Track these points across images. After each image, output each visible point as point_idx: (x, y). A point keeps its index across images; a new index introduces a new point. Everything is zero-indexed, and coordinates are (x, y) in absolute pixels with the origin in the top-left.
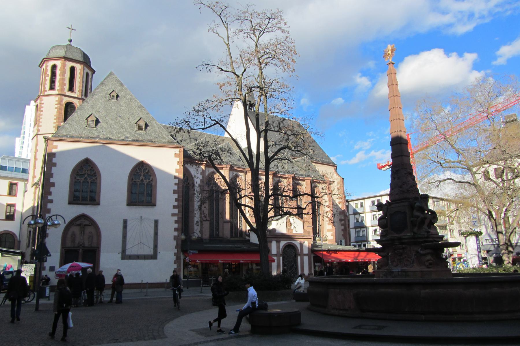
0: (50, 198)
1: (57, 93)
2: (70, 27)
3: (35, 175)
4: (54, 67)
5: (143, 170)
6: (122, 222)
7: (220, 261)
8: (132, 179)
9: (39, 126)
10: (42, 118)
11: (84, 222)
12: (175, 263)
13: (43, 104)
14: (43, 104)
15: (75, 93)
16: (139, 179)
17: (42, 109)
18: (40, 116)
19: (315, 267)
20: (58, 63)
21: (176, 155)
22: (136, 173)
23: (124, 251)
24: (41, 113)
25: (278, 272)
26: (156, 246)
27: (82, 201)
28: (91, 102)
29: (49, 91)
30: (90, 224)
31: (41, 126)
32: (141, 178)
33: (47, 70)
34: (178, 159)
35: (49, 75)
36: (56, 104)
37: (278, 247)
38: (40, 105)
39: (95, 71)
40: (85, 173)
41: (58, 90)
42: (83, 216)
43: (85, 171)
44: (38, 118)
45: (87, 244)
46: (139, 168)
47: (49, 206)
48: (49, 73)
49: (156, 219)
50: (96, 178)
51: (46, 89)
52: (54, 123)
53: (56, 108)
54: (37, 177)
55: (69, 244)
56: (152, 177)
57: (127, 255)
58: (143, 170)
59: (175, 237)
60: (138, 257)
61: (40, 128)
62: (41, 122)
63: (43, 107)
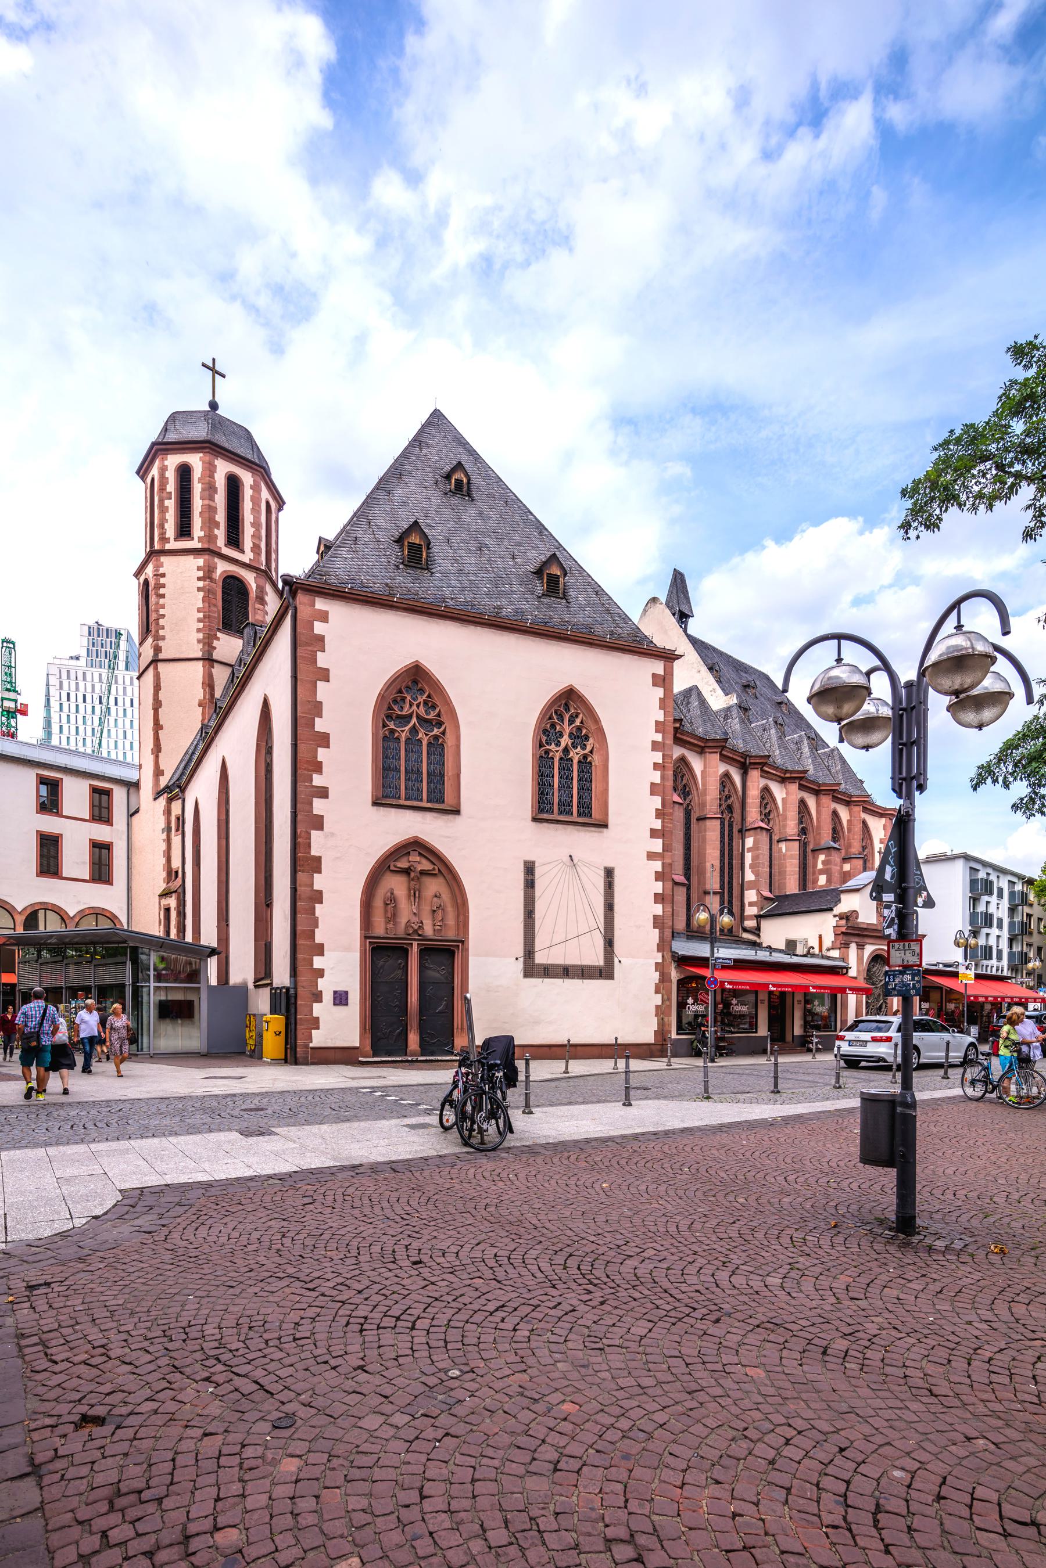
0: (317, 780)
1: (199, 546)
3: (161, 768)
4: (184, 473)
5: (567, 717)
6: (521, 868)
7: (812, 990)
8: (541, 745)
10: (163, 616)
11: (419, 863)
13: (163, 575)
14: (163, 575)
15: (243, 552)
16: (558, 744)
17: (162, 591)
18: (157, 611)
23: (529, 953)
24: (162, 601)
26: (609, 943)
27: (406, 799)
28: (400, 491)
29: (175, 540)
30: (434, 869)
31: (163, 638)
32: (563, 744)
36: (199, 579)
37: (860, 959)
38: (157, 580)
40: (410, 716)
41: (200, 539)
42: (416, 846)
43: (411, 706)
44: (153, 616)
46: (556, 712)
47: (319, 806)
48: (171, 487)
49: (610, 865)
50: (441, 730)
52: (199, 630)
53: (199, 589)
55: (380, 929)
56: (591, 740)
57: (540, 965)
58: (567, 717)
59: (656, 918)
60: (566, 972)
61: (161, 643)
63: (163, 586)
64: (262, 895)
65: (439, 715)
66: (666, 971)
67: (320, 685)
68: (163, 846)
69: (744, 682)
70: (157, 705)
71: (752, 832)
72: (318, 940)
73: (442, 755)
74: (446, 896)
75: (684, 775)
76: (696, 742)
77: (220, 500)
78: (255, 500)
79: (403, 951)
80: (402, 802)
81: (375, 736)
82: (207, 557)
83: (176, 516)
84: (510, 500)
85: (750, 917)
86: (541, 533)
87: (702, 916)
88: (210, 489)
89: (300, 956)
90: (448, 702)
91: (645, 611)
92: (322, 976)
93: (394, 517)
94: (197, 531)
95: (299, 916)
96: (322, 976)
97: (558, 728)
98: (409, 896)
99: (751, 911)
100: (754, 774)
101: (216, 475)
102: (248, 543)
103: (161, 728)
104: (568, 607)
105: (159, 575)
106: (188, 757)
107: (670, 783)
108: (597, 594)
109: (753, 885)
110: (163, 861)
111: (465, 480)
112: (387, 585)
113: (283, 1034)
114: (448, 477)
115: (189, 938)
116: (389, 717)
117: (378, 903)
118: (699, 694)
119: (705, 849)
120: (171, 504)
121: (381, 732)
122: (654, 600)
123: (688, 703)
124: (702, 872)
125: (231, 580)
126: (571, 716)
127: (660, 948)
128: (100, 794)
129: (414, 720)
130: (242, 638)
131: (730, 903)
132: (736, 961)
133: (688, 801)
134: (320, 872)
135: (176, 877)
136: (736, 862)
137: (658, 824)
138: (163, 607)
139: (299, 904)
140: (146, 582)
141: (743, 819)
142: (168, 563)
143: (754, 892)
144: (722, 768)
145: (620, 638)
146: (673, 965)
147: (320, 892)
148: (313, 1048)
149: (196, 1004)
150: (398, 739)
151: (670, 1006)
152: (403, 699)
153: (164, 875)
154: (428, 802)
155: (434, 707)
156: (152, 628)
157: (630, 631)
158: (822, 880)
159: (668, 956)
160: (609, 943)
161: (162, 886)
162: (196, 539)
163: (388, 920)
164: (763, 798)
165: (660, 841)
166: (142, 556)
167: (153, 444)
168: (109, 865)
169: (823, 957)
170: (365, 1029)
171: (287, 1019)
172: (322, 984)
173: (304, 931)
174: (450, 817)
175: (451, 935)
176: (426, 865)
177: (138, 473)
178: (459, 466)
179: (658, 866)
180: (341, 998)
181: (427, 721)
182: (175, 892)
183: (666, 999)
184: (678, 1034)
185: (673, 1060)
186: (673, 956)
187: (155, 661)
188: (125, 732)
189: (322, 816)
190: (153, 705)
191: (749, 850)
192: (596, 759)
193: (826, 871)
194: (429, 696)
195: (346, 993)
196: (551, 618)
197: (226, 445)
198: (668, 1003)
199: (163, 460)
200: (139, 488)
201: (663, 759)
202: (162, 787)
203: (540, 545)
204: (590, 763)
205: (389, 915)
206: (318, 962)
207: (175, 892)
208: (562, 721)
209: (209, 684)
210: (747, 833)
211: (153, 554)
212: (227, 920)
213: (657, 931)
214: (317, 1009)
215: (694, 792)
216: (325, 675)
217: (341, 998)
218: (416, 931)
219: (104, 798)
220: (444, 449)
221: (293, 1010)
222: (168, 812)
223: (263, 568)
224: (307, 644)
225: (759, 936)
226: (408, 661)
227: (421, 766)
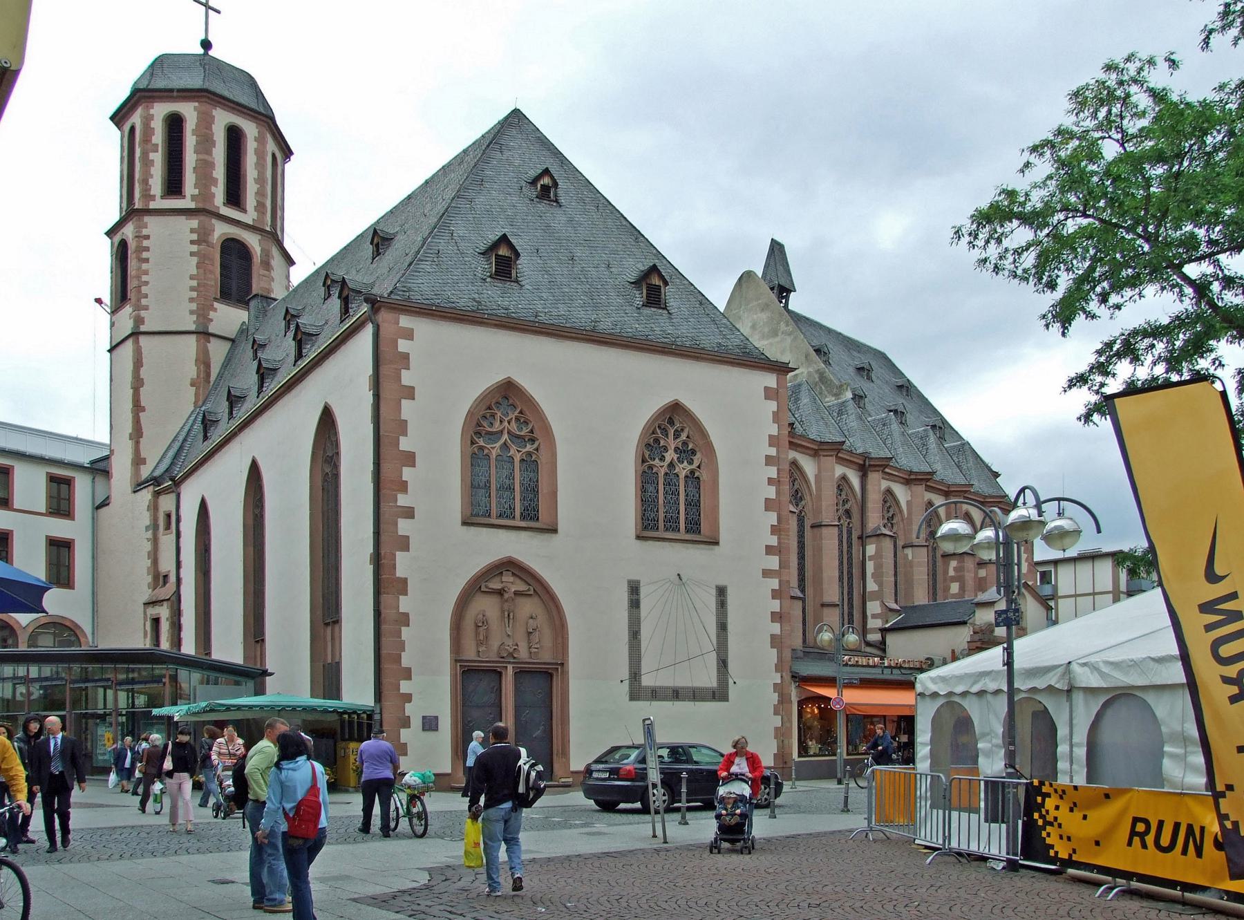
1: (192, 205)
3: (143, 455)
4: (175, 124)
5: (671, 432)
8: (643, 461)
10: (146, 283)
13: (147, 237)
15: (244, 211)
16: (662, 459)
17: (145, 255)
18: (138, 277)
20: (189, 111)
21: (769, 394)
23: (635, 675)
24: (144, 266)
25: (475, 748)
26: (723, 664)
27: (497, 518)
28: (482, 199)
29: (162, 197)
30: (529, 590)
31: (146, 308)
33: (148, 131)
35: (157, 145)
36: (192, 242)
39: (291, 153)
40: (502, 432)
41: (193, 198)
44: (132, 284)
45: (523, 654)
46: (659, 427)
48: (158, 138)
49: (721, 583)
50: (535, 446)
51: (152, 193)
52: (191, 300)
53: (192, 254)
56: (698, 455)
58: (671, 432)
61: (143, 313)
65: (532, 431)
68: (148, 546)
69: (858, 363)
71: (874, 539)
74: (542, 620)
76: (809, 445)
77: (219, 154)
78: (260, 154)
82: (202, 218)
85: (873, 631)
87: (826, 636)
92: (410, 701)
98: (503, 617)
99: (873, 623)
100: (873, 477)
102: (250, 200)
103: (143, 409)
105: (140, 237)
107: (786, 497)
109: (878, 596)
110: (149, 563)
112: (474, 299)
114: (534, 182)
115: (165, 645)
120: (158, 158)
124: (818, 581)
126: (676, 431)
129: (505, 436)
131: (851, 615)
133: (800, 507)
136: (856, 571)
137: (774, 541)
138: (146, 273)
142: (153, 225)
143: (878, 603)
144: (839, 470)
147: (406, 615)
152: (493, 416)
153: (149, 579)
156: (131, 295)
157: (737, 342)
158: (955, 588)
159: (788, 677)
160: (723, 664)
161: (146, 594)
163: (479, 643)
164: (885, 501)
165: (776, 559)
168: (70, 568)
172: (409, 709)
174: (546, 536)
175: (546, 657)
176: (521, 587)
178: (546, 172)
179: (774, 583)
181: (518, 437)
183: (786, 721)
185: (797, 783)
187: (135, 334)
189: (408, 537)
191: (871, 558)
192: (704, 475)
193: (959, 579)
194: (521, 412)
195: (436, 718)
197: (226, 93)
199: (148, 108)
200: (114, 136)
201: (778, 474)
204: (698, 478)
205: (481, 638)
208: (667, 435)
209: (204, 362)
210: (868, 540)
211: (131, 213)
215: (807, 497)
218: (511, 655)
219: (64, 487)
222: (154, 507)
223: (268, 229)
226: (499, 377)
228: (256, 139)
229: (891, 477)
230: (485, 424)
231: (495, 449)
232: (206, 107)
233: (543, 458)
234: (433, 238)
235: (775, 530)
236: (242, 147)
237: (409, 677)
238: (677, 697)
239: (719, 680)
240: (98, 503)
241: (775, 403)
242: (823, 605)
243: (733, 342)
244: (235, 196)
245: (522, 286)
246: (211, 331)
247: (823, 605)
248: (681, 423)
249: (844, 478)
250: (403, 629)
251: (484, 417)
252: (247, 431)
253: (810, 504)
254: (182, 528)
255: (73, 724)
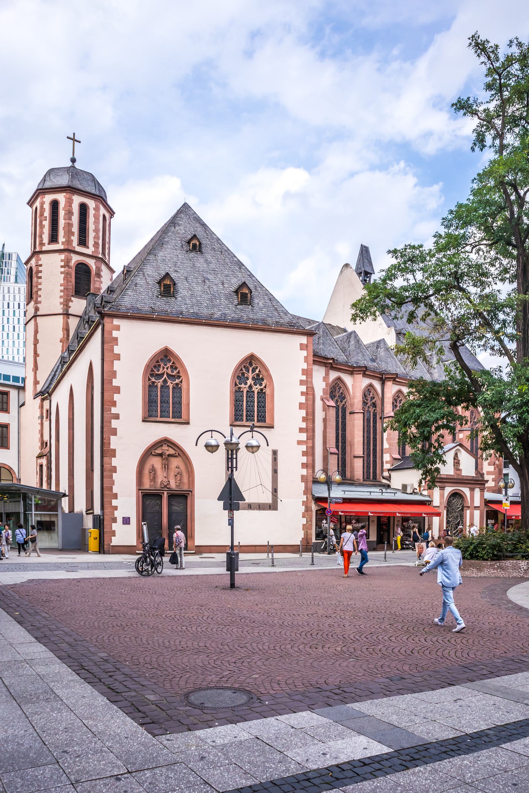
0: (114, 410)
2: (72, 137)
3: (38, 380)
4: (55, 205)
5: (251, 369)
7: (398, 515)
8: (236, 385)
9: (37, 302)
10: (40, 289)
12: (304, 516)
13: (41, 265)
14: (41, 265)
15: (88, 248)
16: (246, 384)
17: (40, 275)
19: (487, 525)
21: (302, 347)
22: (240, 374)
24: (40, 280)
26: (275, 491)
27: (161, 417)
28: (161, 254)
29: (48, 244)
30: (176, 453)
31: (40, 302)
33: (43, 210)
34: (304, 353)
35: (46, 217)
36: (62, 267)
37: (442, 496)
38: (38, 268)
39: (114, 213)
40: (163, 374)
41: (63, 243)
42: (166, 441)
43: (164, 368)
44: (34, 290)
46: (244, 367)
47: (114, 423)
51: (44, 242)
52: (61, 297)
53: (62, 273)
54: (40, 382)
55: (147, 485)
56: (265, 381)
58: (251, 369)
61: (39, 305)
62: (40, 296)
63: (41, 272)
64: (90, 465)
65: (179, 372)
66: (308, 505)
67: (115, 362)
68: (39, 427)
70: (36, 342)
72: (114, 491)
73: (181, 393)
75: (340, 388)
77: (75, 219)
78: (96, 217)
79: (159, 496)
80: (159, 419)
81: (144, 386)
82: (66, 254)
83: (49, 230)
84: (224, 251)
86: (240, 268)
88: (69, 213)
89: (105, 500)
90: (183, 366)
91: (341, 272)
92: (117, 509)
93: (158, 268)
94: (61, 238)
95: (104, 479)
96: (117, 509)
97: (246, 375)
99: (387, 466)
101: (73, 205)
102: (91, 242)
103: (38, 356)
104: (252, 309)
106: (53, 373)
108: (270, 300)
111: (198, 244)
112: (151, 307)
113: (98, 539)
114: (189, 243)
116: (152, 375)
117: (146, 471)
118: (356, 336)
119: (354, 431)
121: (147, 383)
122: (347, 265)
123: (349, 342)
124: (352, 445)
125: (80, 266)
127: (305, 493)
128: (2, 395)
129: (165, 376)
130: (86, 299)
132: (344, 499)
133: (343, 403)
134: (115, 457)
135: (46, 446)
137: (304, 425)
139: (104, 473)
140: (31, 269)
141: (383, 411)
145: (282, 325)
146: (313, 502)
147: (115, 467)
148: (112, 546)
149: (56, 522)
150: (157, 386)
151: (311, 525)
152: (160, 366)
154: (173, 418)
155: (176, 368)
156: (34, 296)
159: (310, 497)
160: (275, 491)
161: (38, 451)
162: (60, 243)
163: (151, 481)
165: (305, 435)
166: (29, 254)
167: (38, 190)
169: (421, 494)
170: (139, 536)
171: (100, 531)
172: (117, 514)
173: (107, 487)
175: (186, 488)
177: (28, 204)
178: (195, 237)
180: (126, 521)
182: (45, 455)
183: (309, 521)
184: (316, 540)
186: (313, 497)
187: (35, 316)
188: (14, 327)
190: (34, 342)
192: (268, 391)
194: (173, 363)
195: (129, 518)
196: (242, 316)
197: (80, 187)
198: (310, 523)
199: (42, 198)
200: (29, 211)
202: (38, 391)
203: (240, 275)
204: (265, 393)
206: (114, 503)
207: (45, 455)
208: (248, 371)
209: (67, 329)
211: (35, 253)
212: (73, 476)
213: (303, 483)
214: (114, 526)
215: (348, 397)
216: (118, 357)
217: (126, 521)
218: (165, 486)
219: (5, 396)
220: (188, 226)
221: (102, 527)
222: (42, 407)
223: (100, 256)
224: (109, 342)
225: (389, 481)
226: (161, 347)
227: (169, 400)
228: (94, 209)
229: (401, 383)
230: (155, 370)
231: (159, 383)
232: (68, 195)
233: (184, 385)
234: (135, 277)
235: (304, 419)
236: (87, 214)
237: (116, 498)
238: (251, 508)
239: (273, 499)
240: (20, 404)
241: (306, 352)
242: (355, 457)
243: (286, 319)
244: (83, 242)
245: (176, 298)
246: (70, 312)
247: (355, 457)
248: (255, 364)
249: (371, 385)
250: (114, 474)
251: (155, 367)
252: (70, 370)
253: (349, 401)
254: (52, 418)
255: (30, 518)
